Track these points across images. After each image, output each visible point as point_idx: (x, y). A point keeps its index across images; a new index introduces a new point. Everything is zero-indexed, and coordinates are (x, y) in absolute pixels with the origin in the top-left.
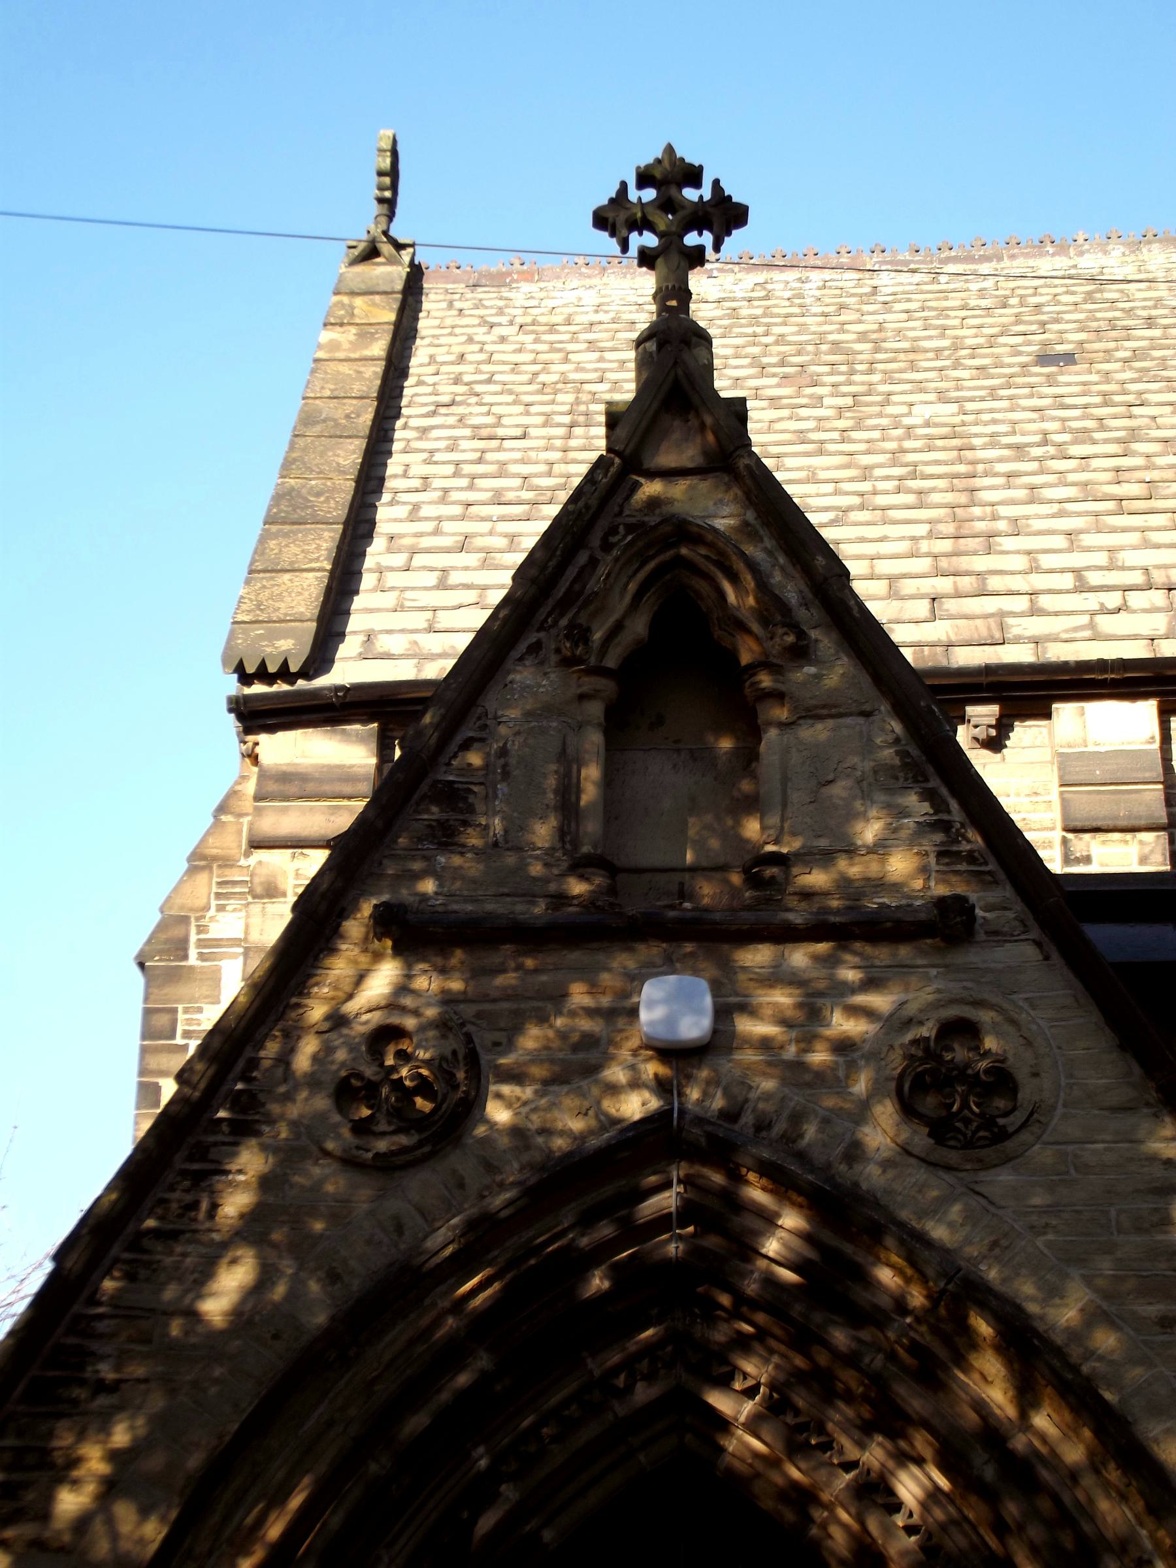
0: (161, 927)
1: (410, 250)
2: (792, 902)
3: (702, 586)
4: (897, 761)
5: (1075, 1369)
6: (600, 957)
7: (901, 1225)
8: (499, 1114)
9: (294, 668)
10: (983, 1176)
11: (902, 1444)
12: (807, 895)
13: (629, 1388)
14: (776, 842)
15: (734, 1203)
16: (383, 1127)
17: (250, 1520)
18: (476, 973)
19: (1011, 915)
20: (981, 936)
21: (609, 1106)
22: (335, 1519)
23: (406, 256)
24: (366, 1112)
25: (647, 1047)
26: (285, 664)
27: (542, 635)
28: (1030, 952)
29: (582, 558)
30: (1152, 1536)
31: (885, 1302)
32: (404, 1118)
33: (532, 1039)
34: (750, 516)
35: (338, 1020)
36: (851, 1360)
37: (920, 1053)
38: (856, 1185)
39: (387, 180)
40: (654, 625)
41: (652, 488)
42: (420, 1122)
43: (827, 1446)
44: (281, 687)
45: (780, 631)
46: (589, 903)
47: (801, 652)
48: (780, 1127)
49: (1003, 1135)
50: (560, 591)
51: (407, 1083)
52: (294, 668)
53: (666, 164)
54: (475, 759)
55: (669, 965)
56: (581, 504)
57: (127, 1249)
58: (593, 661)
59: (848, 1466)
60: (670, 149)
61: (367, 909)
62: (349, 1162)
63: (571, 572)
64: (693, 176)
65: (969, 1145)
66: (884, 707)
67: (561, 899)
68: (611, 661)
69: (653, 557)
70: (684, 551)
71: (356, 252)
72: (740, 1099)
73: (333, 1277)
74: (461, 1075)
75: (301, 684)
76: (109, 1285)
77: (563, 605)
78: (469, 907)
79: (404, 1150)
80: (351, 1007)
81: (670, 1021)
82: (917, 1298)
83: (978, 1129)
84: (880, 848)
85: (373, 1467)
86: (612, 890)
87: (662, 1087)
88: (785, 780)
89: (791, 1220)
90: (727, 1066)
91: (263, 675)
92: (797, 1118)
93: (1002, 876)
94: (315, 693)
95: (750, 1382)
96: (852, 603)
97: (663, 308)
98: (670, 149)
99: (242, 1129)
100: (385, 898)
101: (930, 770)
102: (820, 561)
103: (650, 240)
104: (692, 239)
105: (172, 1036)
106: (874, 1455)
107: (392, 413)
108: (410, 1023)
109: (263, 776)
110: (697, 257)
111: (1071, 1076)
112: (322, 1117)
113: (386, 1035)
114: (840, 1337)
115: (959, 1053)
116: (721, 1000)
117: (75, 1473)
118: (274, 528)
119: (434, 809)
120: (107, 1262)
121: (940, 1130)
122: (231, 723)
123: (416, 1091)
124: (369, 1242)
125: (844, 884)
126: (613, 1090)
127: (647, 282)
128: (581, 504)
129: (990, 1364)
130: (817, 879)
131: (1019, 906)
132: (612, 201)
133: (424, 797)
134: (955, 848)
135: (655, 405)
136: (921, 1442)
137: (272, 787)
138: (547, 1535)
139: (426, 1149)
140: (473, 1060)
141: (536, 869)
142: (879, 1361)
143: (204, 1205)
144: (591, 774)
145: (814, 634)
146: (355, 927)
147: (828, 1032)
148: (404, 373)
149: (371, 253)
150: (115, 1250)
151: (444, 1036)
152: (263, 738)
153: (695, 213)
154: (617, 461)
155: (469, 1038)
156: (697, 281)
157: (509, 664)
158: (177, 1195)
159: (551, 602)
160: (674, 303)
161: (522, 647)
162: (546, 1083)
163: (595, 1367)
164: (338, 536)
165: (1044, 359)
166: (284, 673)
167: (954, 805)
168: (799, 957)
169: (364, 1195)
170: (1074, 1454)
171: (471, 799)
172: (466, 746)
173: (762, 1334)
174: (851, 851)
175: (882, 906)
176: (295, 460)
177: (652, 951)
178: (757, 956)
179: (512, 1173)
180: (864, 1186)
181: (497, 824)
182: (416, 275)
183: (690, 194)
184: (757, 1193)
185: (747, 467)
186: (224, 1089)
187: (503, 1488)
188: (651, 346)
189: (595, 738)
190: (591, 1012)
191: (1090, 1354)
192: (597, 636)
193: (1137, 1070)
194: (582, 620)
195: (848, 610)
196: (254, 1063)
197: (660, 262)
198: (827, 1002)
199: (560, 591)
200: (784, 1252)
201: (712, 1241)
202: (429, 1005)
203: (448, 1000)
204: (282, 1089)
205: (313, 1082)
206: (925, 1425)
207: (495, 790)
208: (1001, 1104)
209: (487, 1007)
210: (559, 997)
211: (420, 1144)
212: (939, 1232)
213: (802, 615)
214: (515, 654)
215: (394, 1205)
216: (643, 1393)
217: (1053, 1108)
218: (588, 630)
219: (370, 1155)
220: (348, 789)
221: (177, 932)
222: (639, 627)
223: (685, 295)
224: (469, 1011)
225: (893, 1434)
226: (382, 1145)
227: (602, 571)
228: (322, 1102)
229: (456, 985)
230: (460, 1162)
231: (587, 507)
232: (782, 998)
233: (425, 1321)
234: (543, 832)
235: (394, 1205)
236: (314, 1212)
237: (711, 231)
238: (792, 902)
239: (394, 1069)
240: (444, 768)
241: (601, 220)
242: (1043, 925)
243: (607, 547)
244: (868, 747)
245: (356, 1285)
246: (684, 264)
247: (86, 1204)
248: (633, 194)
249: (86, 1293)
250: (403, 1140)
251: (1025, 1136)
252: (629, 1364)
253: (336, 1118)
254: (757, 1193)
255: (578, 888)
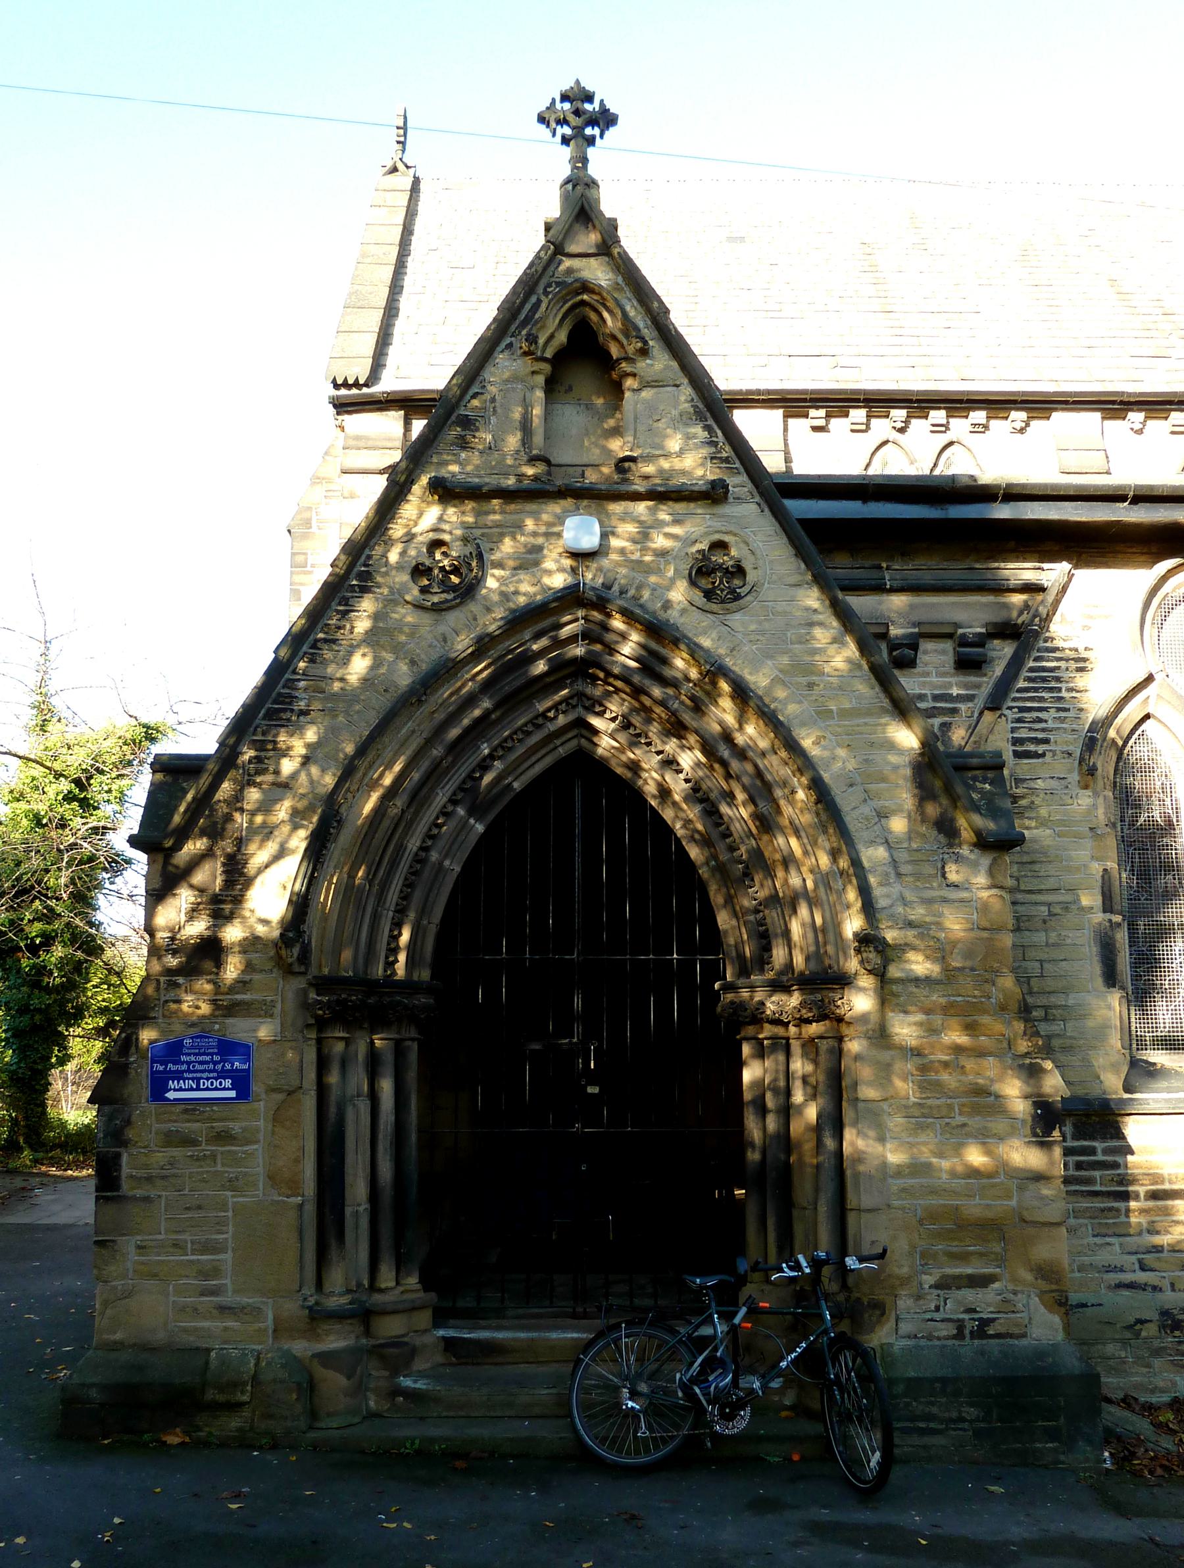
0: (298, 512)
1: (413, 169)
2: (637, 481)
3: (593, 316)
4: (692, 410)
5: (768, 706)
6: (543, 506)
7: (689, 639)
8: (491, 583)
9: (361, 382)
10: (728, 617)
11: (684, 742)
12: (646, 477)
13: (555, 718)
14: (631, 451)
15: (606, 628)
16: (436, 590)
17: (375, 776)
18: (478, 514)
19: (746, 489)
20: (731, 500)
21: (547, 581)
22: (416, 776)
23: (412, 171)
24: (427, 583)
25: (567, 552)
26: (357, 379)
27: (513, 339)
28: (754, 507)
29: (533, 299)
30: (799, 780)
31: (679, 675)
32: (447, 587)
33: (507, 546)
34: (620, 280)
35: (409, 537)
36: (662, 703)
37: (700, 557)
38: (668, 621)
39: (401, 132)
40: (570, 337)
41: (567, 263)
42: (454, 588)
43: (649, 744)
44: (354, 391)
45: (634, 340)
46: (536, 478)
47: (644, 352)
48: (632, 592)
49: (738, 597)
50: (522, 316)
51: (447, 568)
52: (361, 382)
53: (576, 89)
54: (476, 403)
55: (576, 511)
56: (533, 270)
57: (311, 648)
58: (539, 354)
59: (659, 753)
60: (578, 82)
61: (424, 480)
62: (418, 607)
63: (528, 306)
64: (589, 98)
65: (722, 602)
66: (686, 381)
67: (520, 477)
68: (549, 354)
69: (569, 300)
70: (585, 297)
71: (386, 169)
72: (612, 578)
73: (413, 663)
74: (474, 564)
75: (365, 390)
76: (302, 665)
77: (524, 324)
78: (477, 480)
79: (446, 601)
80: (414, 530)
81: (576, 539)
82: (694, 674)
83: (728, 593)
84: (680, 453)
85: (435, 752)
86: (549, 473)
87: (574, 570)
88: (636, 418)
89: (635, 637)
90: (605, 562)
91: (345, 385)
92: (640, 588)
93: (742, 470)
94: (371, 395)
95: (614, 715)
96: (671, 327)
97: (574, 168)
98: (578, 82)
99: (365, 590)
100: (433, 474)
101: (708, 415)
102: (656, 304)
103: (567, 131)
104: (589, 131)
105: (306, 567)
106: (671, 746)
107: (407, 253)
108: (446, 537)
109: (346, 437)
110: (591, 141)
111: (772, 569)
112: (404, 584)
113: (436, 544)
114: (657, 692)
115: (718, 558)
116: (604, 529)
117: (291, 753)
118: (349, 310)
119: (458, 429)
120: (301, 654)
121: (709, 595)
122: (332, 411)
123: (451, 572)
124: (430, 646)
125: (661, 471)
126: (549, 573)
127: (567, 152)
128: (533, 270)
129: (726, 703)
130: (650, 469)
131: (750, 485)
132: (548, 108)
133: (453, 422)
134: (719, 455)
135: (571, 219)
136: (692, 739)
137: (351, 443)
138: (516, 785)
139: (458, 601)
140: (480, 557)
141: (509, 461)
142: (676, 706)
143: (348, 626)
144: (537, 411)
145: (651, 343)
146: (418, 489)
147: (654, 546)
148: (411, 233)
149: (395, 170)
150: (305, 648)
151: (465, 545)
152: (346, 417)
153: (591, 117)
154: (552, 247)
155: (478, 546)
156: (591, 152)
157: (496, 354)
158: (334, 622)
159: (517, 322)
160: (580, 165)
161: (503, 345)
162: (515, 569)
163: (541, 707)
164: (381, 315)
165: (731, 239)
166: (356, 384)
167: (719, 433)
168: (641, 507)
169: (426, 619)
170: (763, 744)
171: (477, 424)
172: (474, 396)
173: (617, 690)
174: (666, 456)
175: (683, 484)
176: (358, 276)
177: (569, 503)
178: (616, 508)
179: (499, 613)
180: (672, 622)
181: (489, 437)
182: (416, 182)
183: (588, 107)
184: (617, 623)
185: (619, 253)
186: (356, 570)
187: (496, 763)
188: (570, 186)
189: (540, 394)
190: (535, 534)
191: (775, 699)
192: (541, 341)
193: (803, 566)
194: (534, 332)
195: (670, 331)
196: (369, 557)
197: (572, 143)
198: (652, 530)
199: (522, 316)
200: (633, 652)
201: (598, 647)
202: (456, 528)
203: (466, 526)
204: (383, 570)
205: (399, 567)
206: (697, 732)
207: (489, 419)
208: (737, 582)
209: (486, 531)
210: (520, 527)
211: (455, 598)
212: (706, 642)
213: (646, 332)
214: (499, 349)
215: (442, 629)
216: (562, 720)
217: (763, 584)
218: (537, 337)
219: (430, 603)
220: (390, 445)
221: (306, 515)
222: (562, 337)
223: (585, 160)
224: (477, 532)
225: (680, 737)
226: (436, 599)
227: (544, 306)
228: (405, 577)
229: (470, 519)
230: (473, 607)
231: (536, 271)
232: (630, 528)
233: (459, 684)
234: (513, 441)
235: (442, 629)
236: (401, 631)
237: (599, 127)
238: (637, 481)
239: (440, 561)
240: (463, 408)
241: (542, 119)
242: (761, 494)
243: (546, 293)
244: (676, 403)
245: (424, 666)
246: (585, 144)
247: (648, 279)
248: (558, 106)
249: (291, 669)
250: (444, 596)
251: (748, 598)
252: (555, 707)
253: (412, 584)
254: (617, 623)
255: (530, 471)
